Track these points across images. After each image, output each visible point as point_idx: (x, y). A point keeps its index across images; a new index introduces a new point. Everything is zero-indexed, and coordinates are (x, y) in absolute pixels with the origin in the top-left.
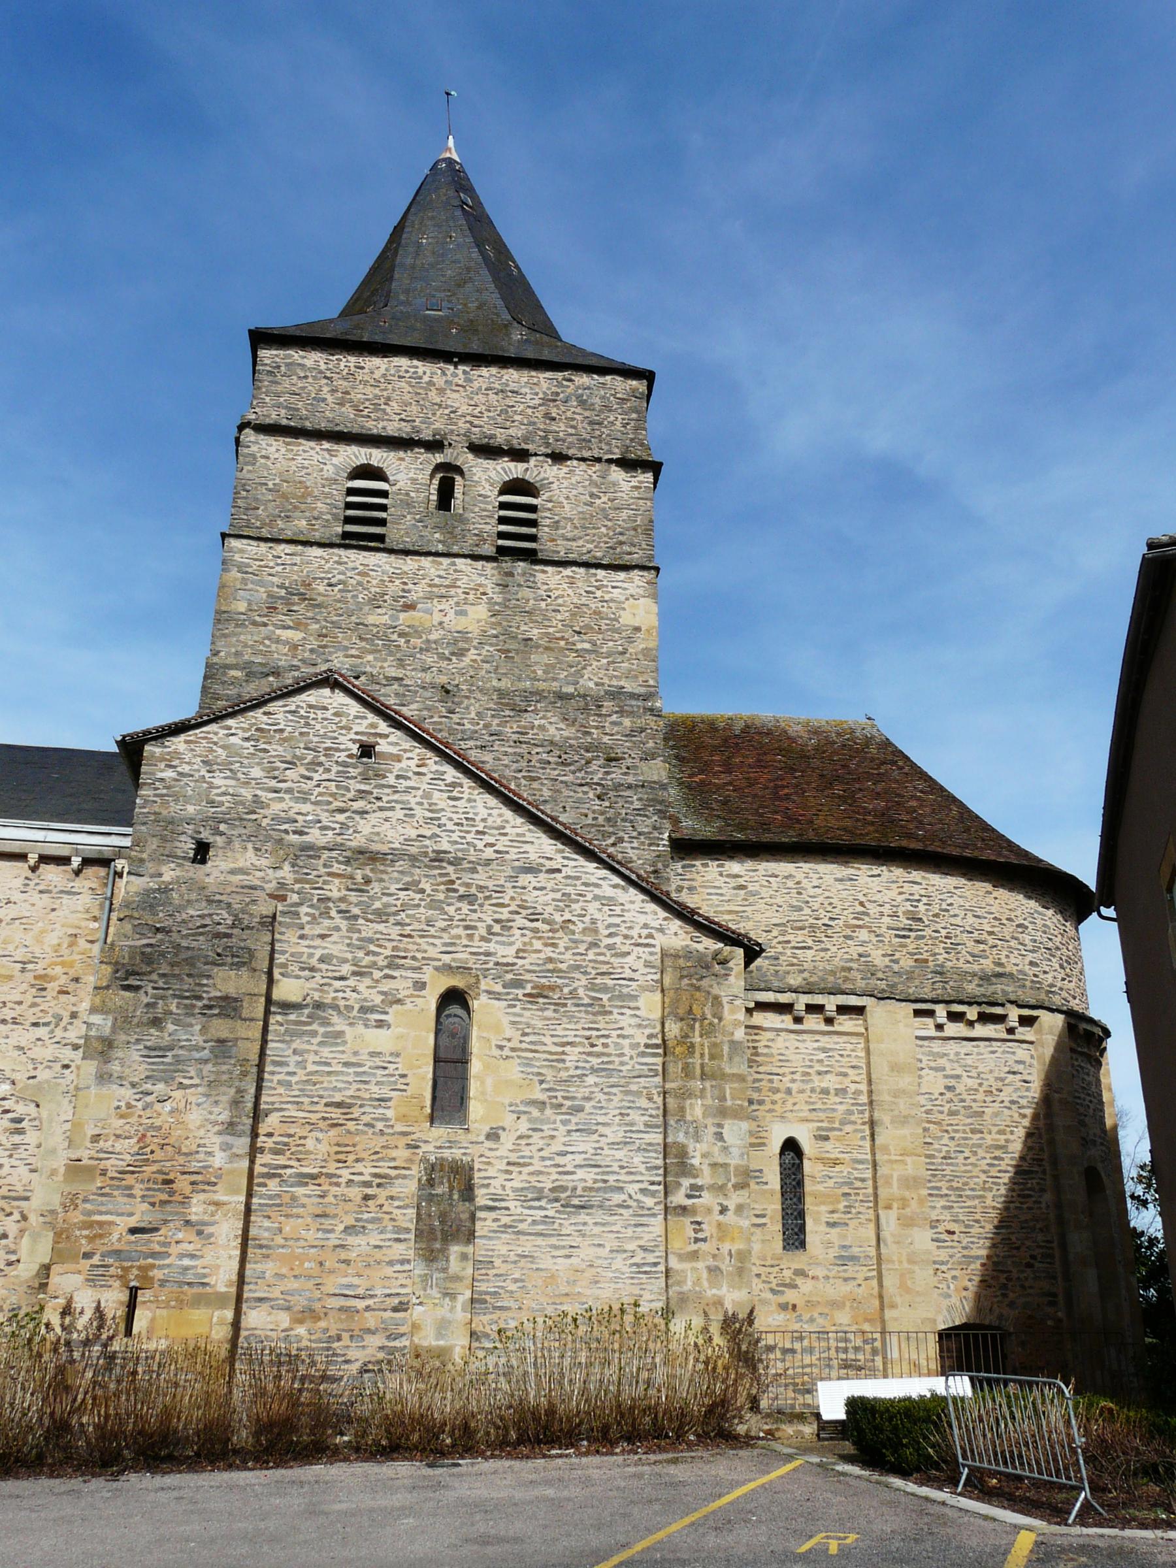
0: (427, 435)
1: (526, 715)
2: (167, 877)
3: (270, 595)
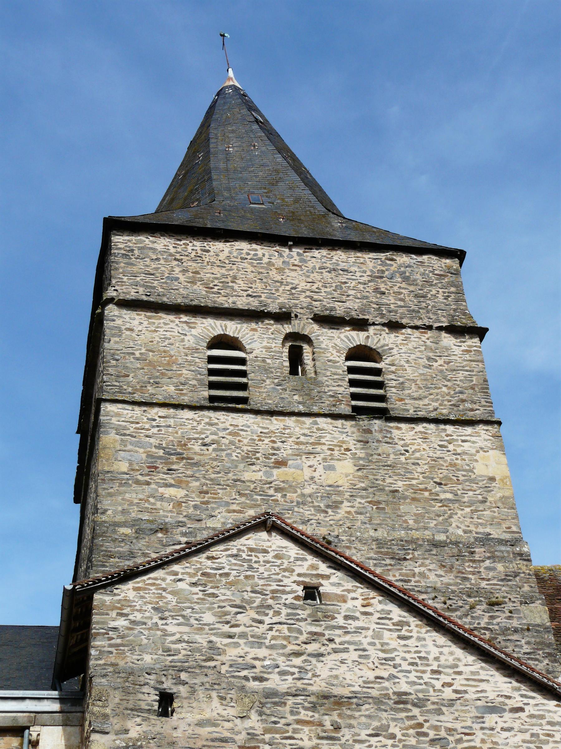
0: (273, 308)
1: (406, 563)
2: (134, 733)
3: (149, 456)
